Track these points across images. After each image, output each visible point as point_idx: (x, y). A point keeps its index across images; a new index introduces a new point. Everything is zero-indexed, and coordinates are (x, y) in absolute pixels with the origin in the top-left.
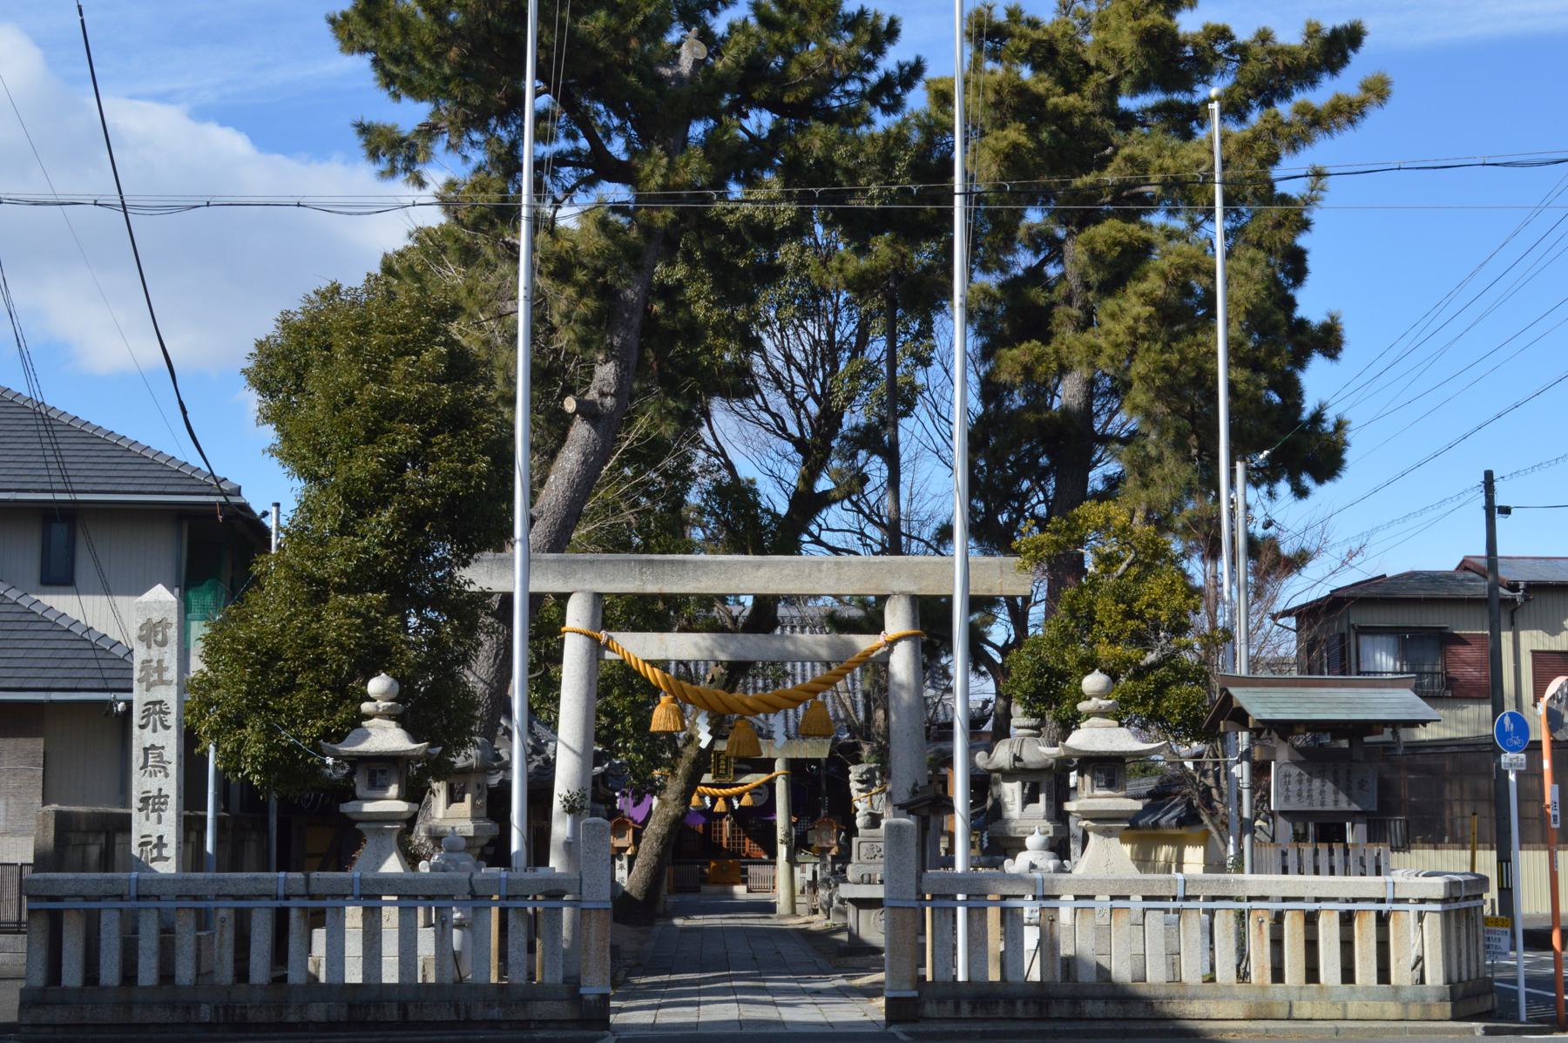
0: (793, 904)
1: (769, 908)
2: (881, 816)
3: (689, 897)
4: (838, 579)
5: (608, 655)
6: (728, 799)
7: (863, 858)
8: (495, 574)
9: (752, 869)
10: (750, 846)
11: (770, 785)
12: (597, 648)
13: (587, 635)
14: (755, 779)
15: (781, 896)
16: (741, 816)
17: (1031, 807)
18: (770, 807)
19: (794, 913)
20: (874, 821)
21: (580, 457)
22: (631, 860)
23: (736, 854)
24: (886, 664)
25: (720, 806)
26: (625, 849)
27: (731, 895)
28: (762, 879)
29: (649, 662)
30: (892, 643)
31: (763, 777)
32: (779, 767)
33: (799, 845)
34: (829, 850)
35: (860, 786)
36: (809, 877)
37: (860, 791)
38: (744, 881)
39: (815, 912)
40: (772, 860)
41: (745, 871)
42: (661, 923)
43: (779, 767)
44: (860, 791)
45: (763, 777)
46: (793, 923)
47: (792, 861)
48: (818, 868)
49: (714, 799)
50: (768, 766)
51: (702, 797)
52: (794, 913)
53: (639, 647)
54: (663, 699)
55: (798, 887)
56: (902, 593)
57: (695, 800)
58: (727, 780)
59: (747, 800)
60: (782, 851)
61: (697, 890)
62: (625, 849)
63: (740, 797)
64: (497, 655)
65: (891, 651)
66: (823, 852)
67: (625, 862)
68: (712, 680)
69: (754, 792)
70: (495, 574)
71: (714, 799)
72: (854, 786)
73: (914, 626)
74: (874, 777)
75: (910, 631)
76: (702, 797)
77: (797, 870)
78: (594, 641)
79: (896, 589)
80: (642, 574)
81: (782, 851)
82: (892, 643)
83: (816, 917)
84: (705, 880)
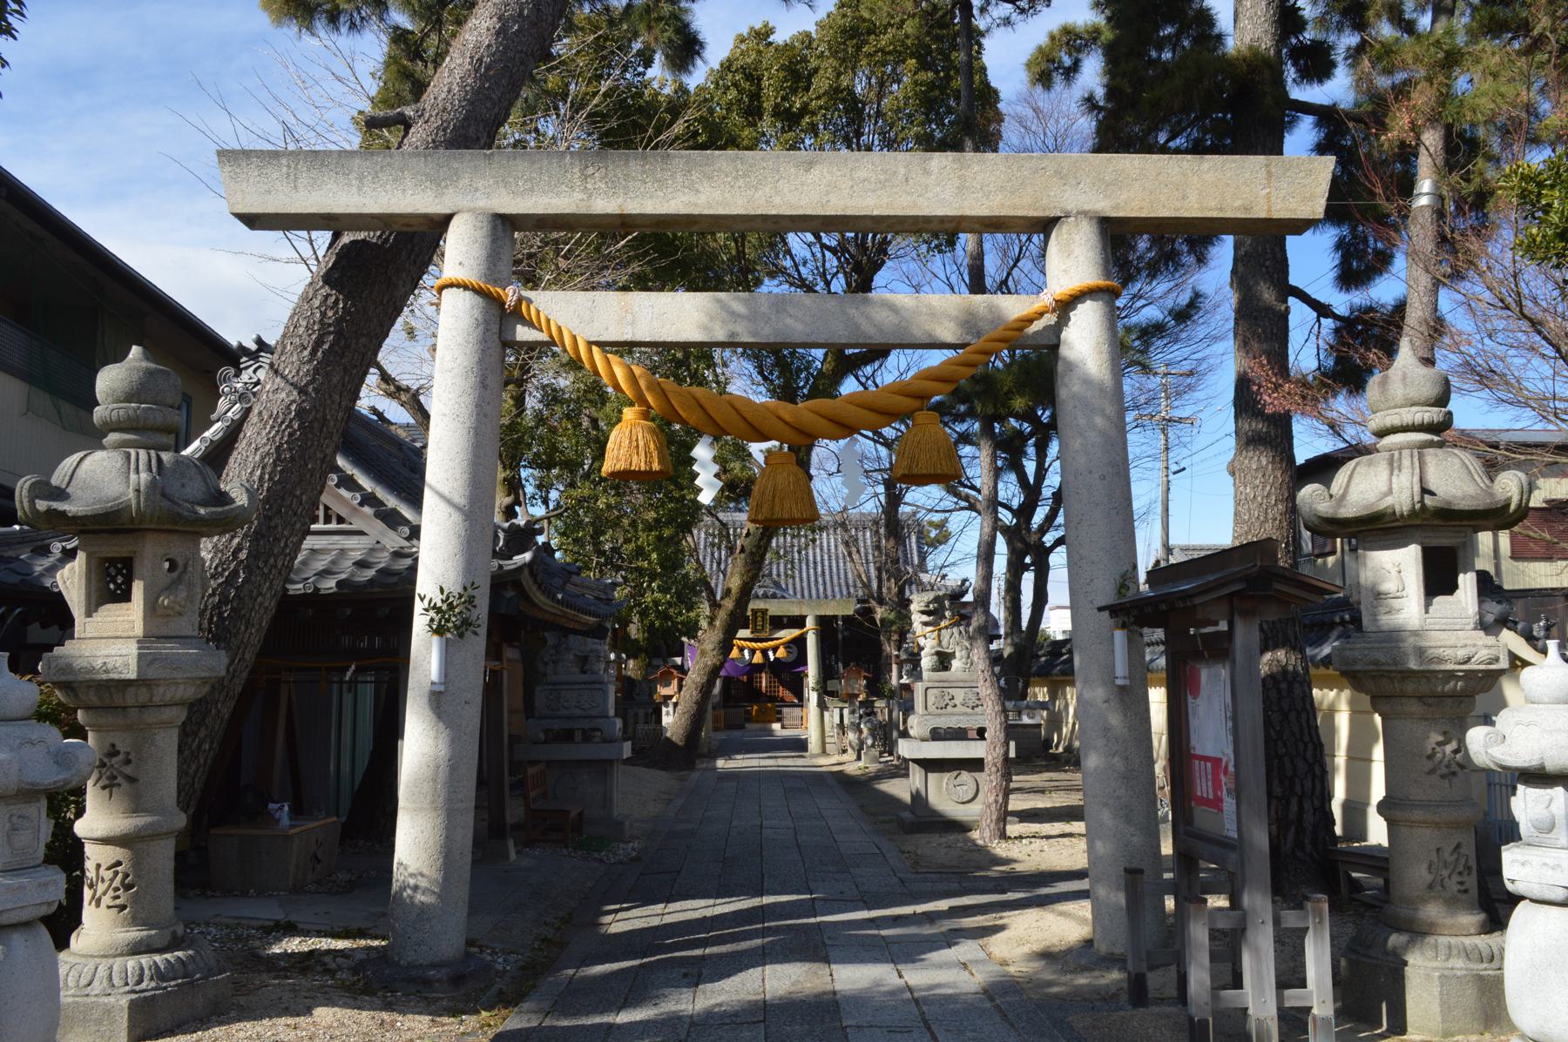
0: (824, 744)
1: (800, 745)
2: (952, 655)
3: (736, 734)
4: (961, 188)
5: (523, 333)
6: (764, 652)
7: (931, 708)
8: (304, 179)
9: (785, 710)
10: (783, 692)
11: (800, 642)
12: (499, 319)
13: (478, 291)
14: (788, 634)
15: (812, 735)
16: (776, 668)
17: (1440, 601)
18: (802, 660)
19: (824, 752)
20: (944, 661)
21: (494, 23)
22: (676, 705)
23: (773, 699)
24: (1055, 348)
25: (758, 658)
26: (671, 697)
27: (771, 732)
28: (794, 718)
29: (601, 344)
30: (1066, 306)
31: (796, 632)
32: (810, 623)
33: (824, 691)
34: (857, 696)
35: (925, 618)
36: (837, 720)
37: (926, 624)
38: (779, 720)
39: (844, 751)
40: (801, 702)
41: (780, 712)
42: (701, 765)
43: (810, 623)
44: (926, 624)
45: (796, 632)
46: (827, 763)
47: (822, 706)
48: (846, 712)
49: (753, 652)
50: (798, 622)
51: (741, 649)
52: (824, 752)
53: (587, 316)
54: (629, 413)
55: (827, 728)
56: (1085, 213)
57: (735, 653)
58: (763, 635)
59: (781, 653)
60: (812, 698)
61: (742, 727)
62: (671, 697)
63: (775, 649)
64: (318, 343)
65: (1063, 320)
66: (851, 697)
67: (671, 709)
68: (748, 534)
69: (788, 645)
70: (304, 179)
71: (753, 652)
72: (917, 619)
73: (1107, 274)
74: (943, 608)
75: (1101, 282)
76: (741, 649)
77: (826, 714)
78: (491, 300)
79: (1071, 206)
80: (585, 178)
81: (812, 698)
82: (1066, 306)
83: (845, 757)
84: (749, 719)
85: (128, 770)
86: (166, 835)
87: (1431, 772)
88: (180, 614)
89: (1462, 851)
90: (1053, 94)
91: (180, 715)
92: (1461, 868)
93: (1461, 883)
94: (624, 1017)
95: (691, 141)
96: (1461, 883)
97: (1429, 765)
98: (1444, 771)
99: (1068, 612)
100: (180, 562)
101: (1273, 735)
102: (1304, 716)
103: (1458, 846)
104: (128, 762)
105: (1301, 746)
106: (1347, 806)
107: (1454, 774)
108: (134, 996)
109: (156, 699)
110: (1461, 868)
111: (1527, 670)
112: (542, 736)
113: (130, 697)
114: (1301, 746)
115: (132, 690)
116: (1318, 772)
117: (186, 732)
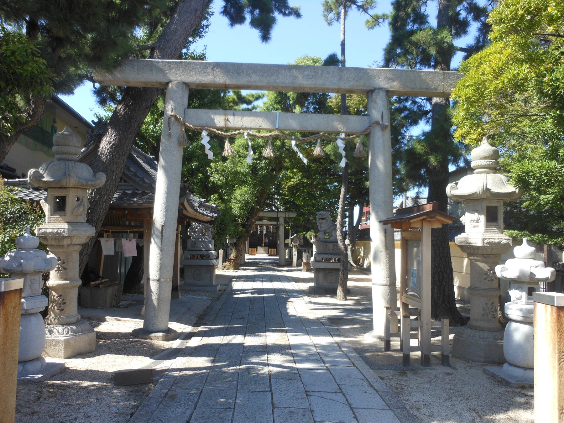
85: (64, 265)
86: (74, 287)
87: (486, 279)
88: (81, 215)
89: (494, 305)
90: (472, 159)
91: (79, 248)
92: (493, 310)
93: (493, 315)
94: (345, 327)
95: (369, 140)
96: (493, 315)
97: (485, 276)
98: (490, 279)
99: (400, 233)
100: (81, 198)
101: (437, 265)
102: (447, 259)
103: (493, 303)
104: (64, 263)
105: (446, 269)
106: (252, 293)
107: (493, 280)
108: (66, 338)
109: (73, 243)
110: (493, 310)
111: (256, 33)
112: (189, 257)
113: (66, 242)
114: (446, 269)
115: (65, 240)
116: (451, 277)
117: (81, 254)
